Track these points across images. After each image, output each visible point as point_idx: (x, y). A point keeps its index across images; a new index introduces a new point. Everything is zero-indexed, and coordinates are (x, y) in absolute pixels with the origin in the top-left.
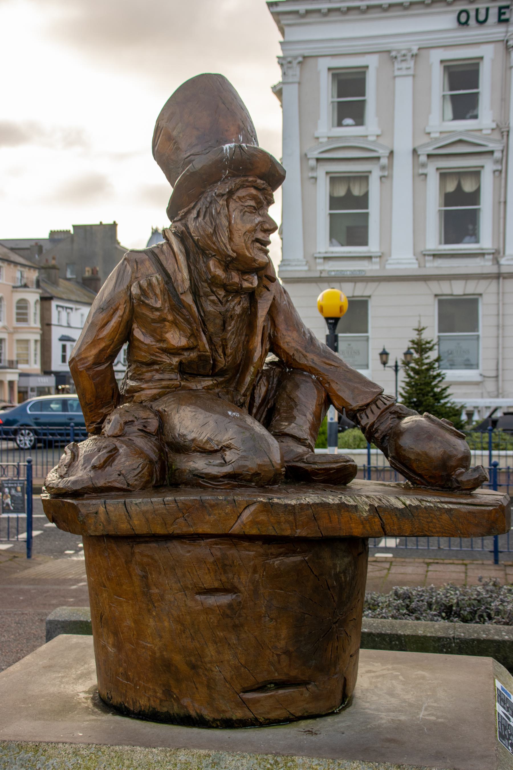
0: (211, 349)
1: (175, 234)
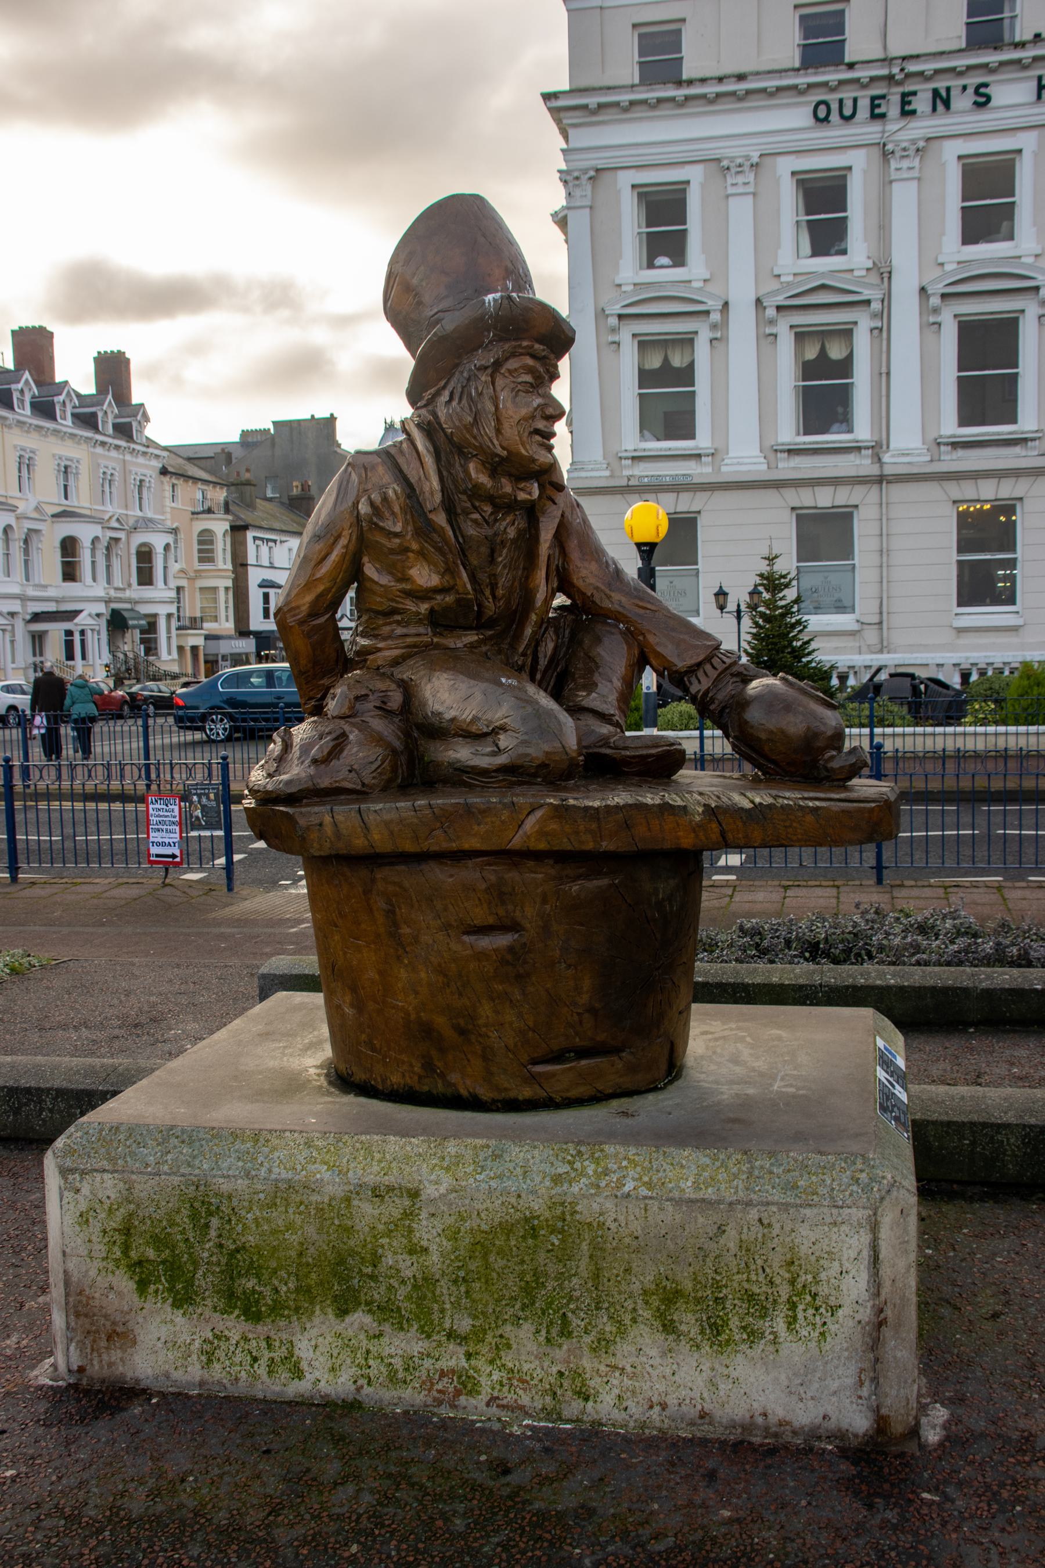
0: (474, 590)
1: (418, 426)
